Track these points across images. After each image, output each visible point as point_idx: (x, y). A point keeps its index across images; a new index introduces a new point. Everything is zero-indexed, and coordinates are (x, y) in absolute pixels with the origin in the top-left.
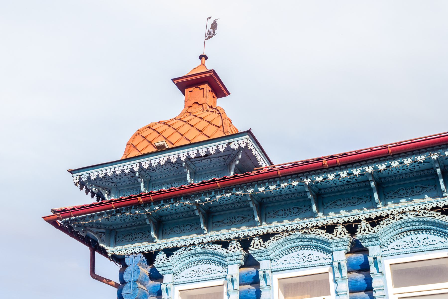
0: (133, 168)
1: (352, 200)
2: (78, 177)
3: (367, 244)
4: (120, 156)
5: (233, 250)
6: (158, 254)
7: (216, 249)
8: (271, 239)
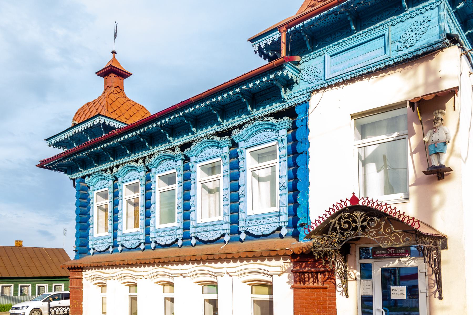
0: (267, 43)
2: (258, 45)
3: (150, 167)
4: (70, 125)
7: (214, 139)
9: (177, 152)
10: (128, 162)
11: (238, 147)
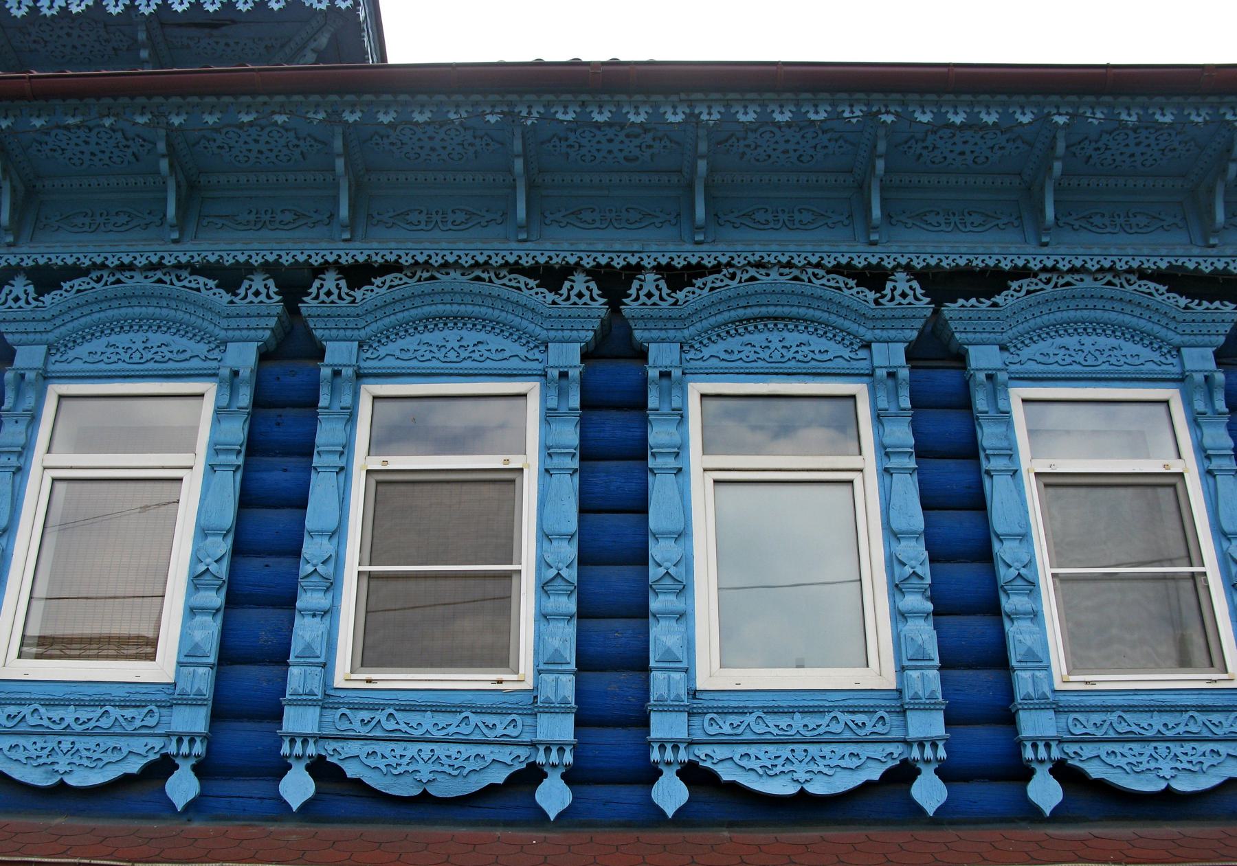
1: (797, 216)
3: (647, 334)
5: (251, 297)
7: (198, 290)
8: (372, 284)
10: (152, 267)
11: (322, 358)
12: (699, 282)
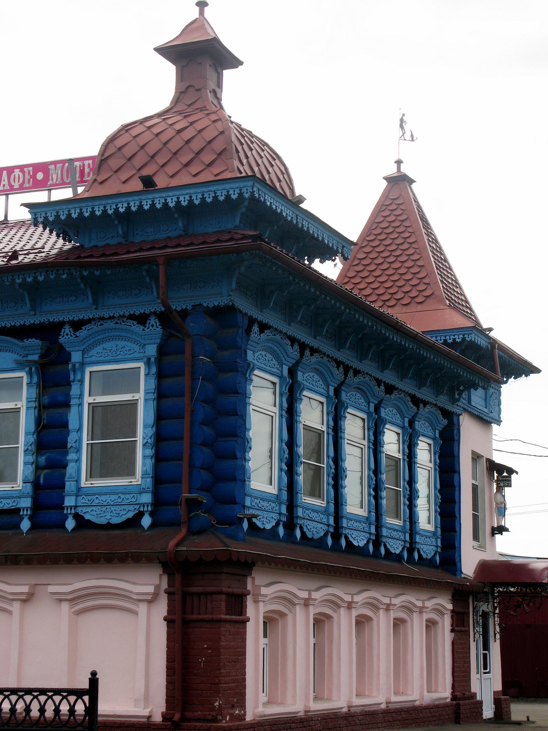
6: (149, 318)
7: (131, 326)
9: (153, 326)
12: (84, 328)
